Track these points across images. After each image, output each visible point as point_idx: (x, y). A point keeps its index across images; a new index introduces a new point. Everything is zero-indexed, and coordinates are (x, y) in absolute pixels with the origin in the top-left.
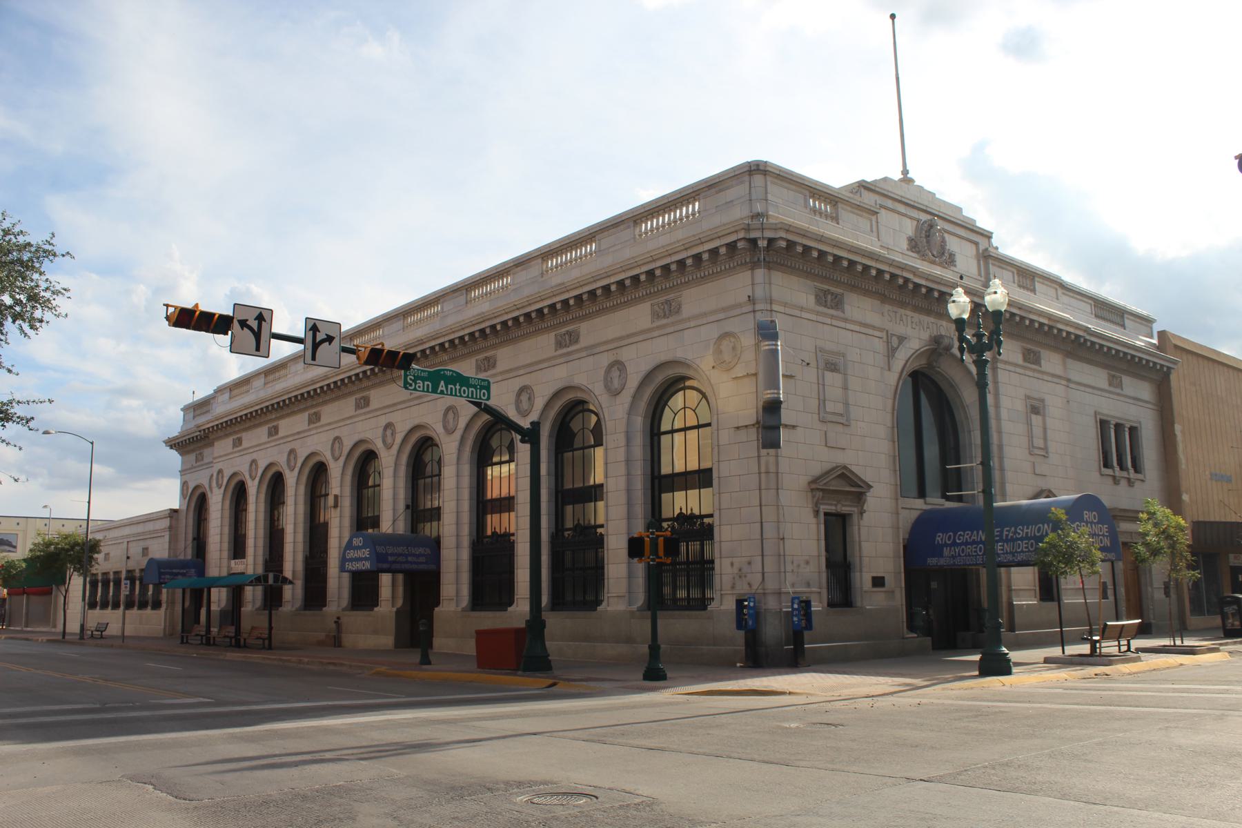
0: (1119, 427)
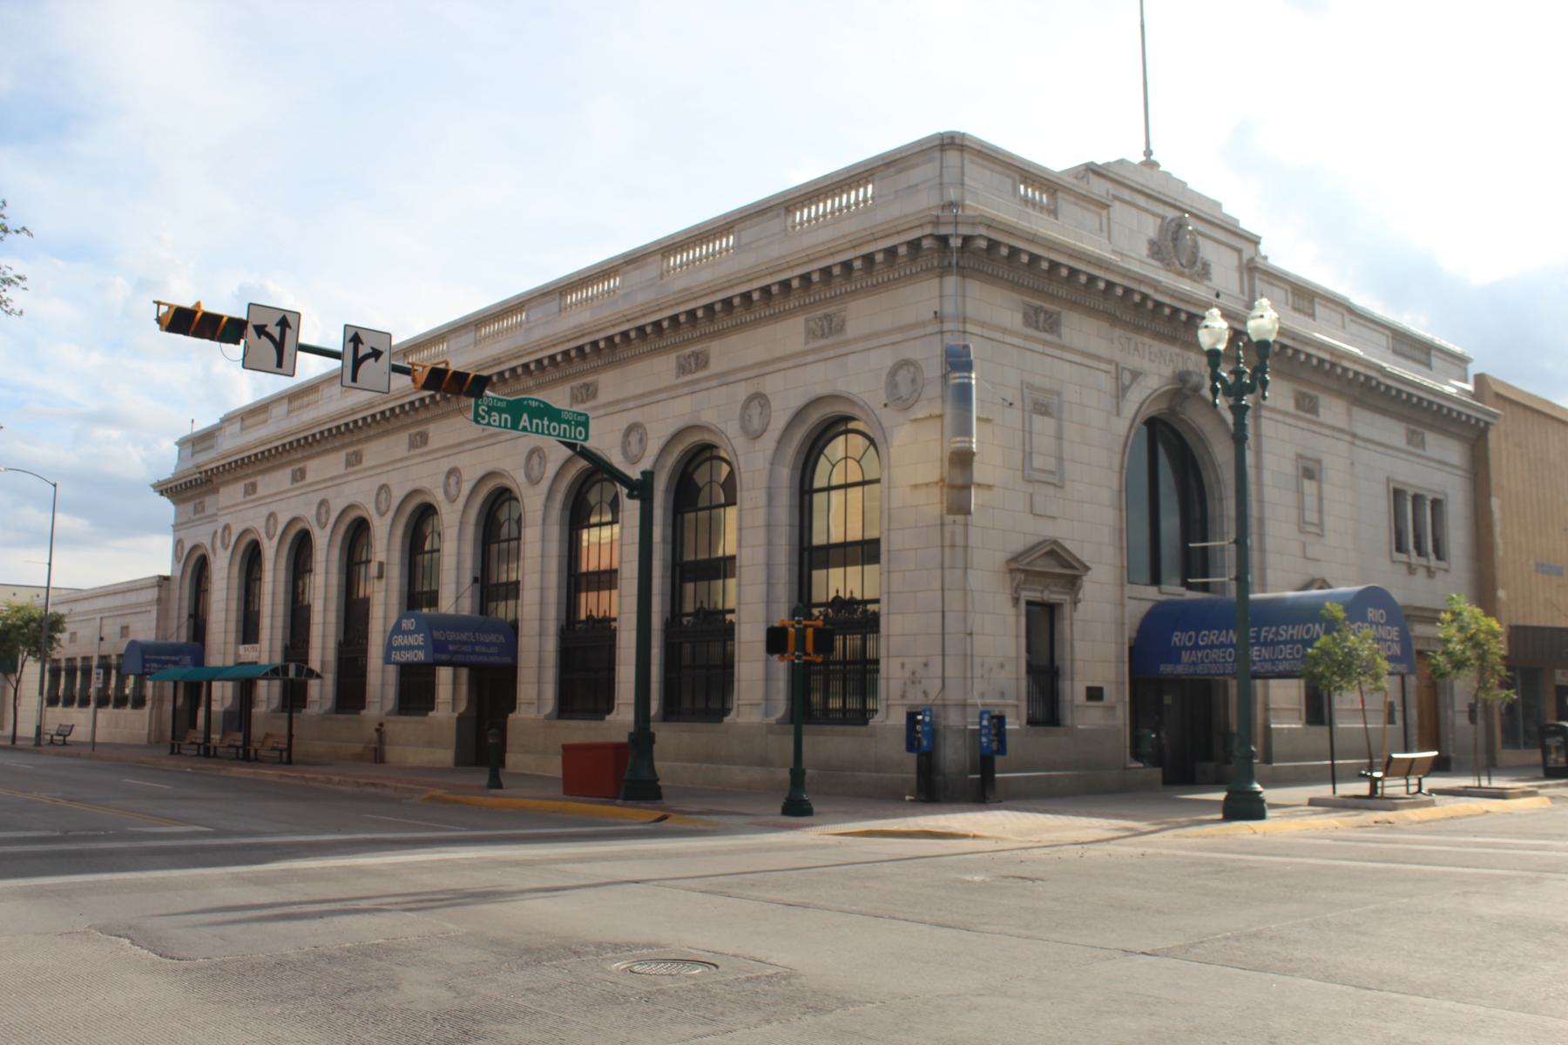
0: (1417, 499)
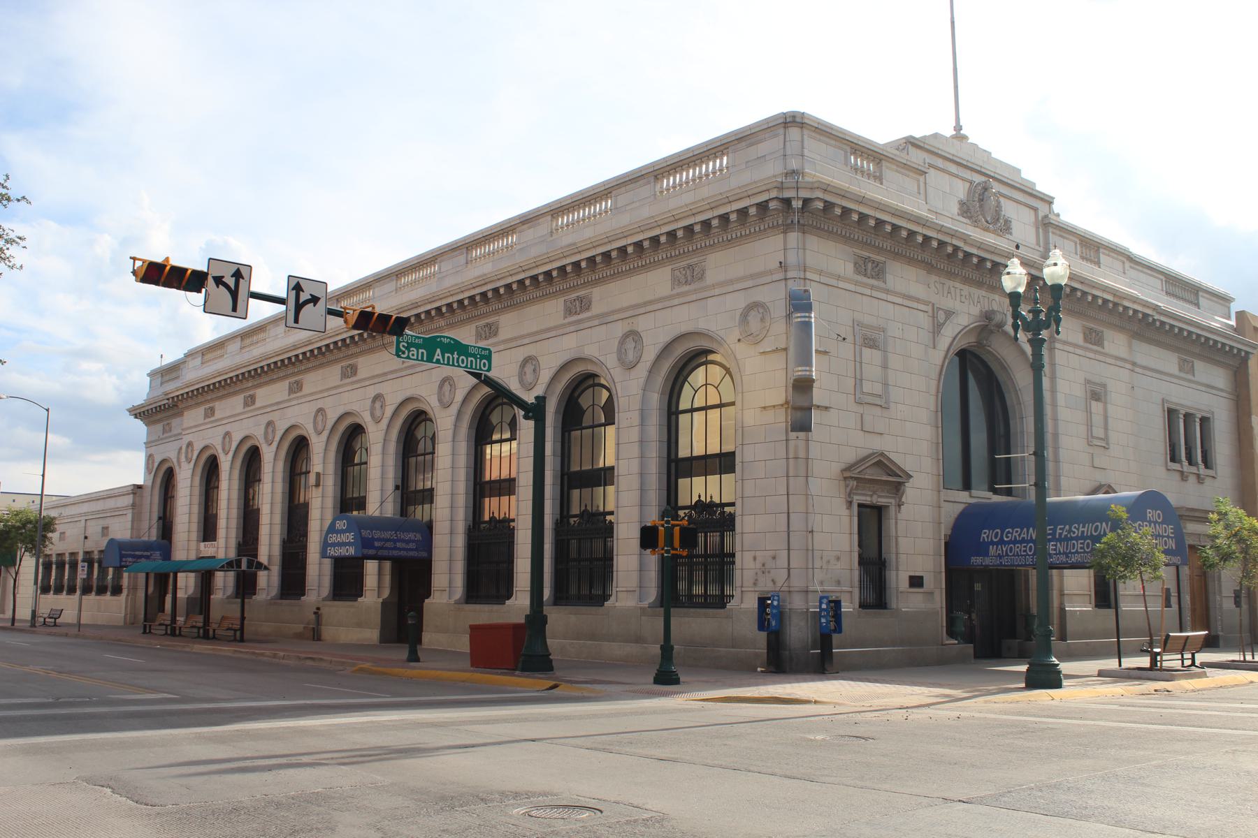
0: (1188, 417)
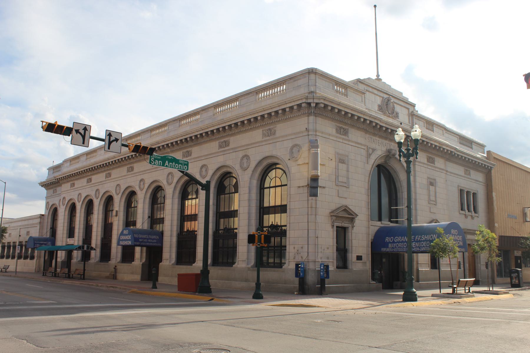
0: (468, 193)
